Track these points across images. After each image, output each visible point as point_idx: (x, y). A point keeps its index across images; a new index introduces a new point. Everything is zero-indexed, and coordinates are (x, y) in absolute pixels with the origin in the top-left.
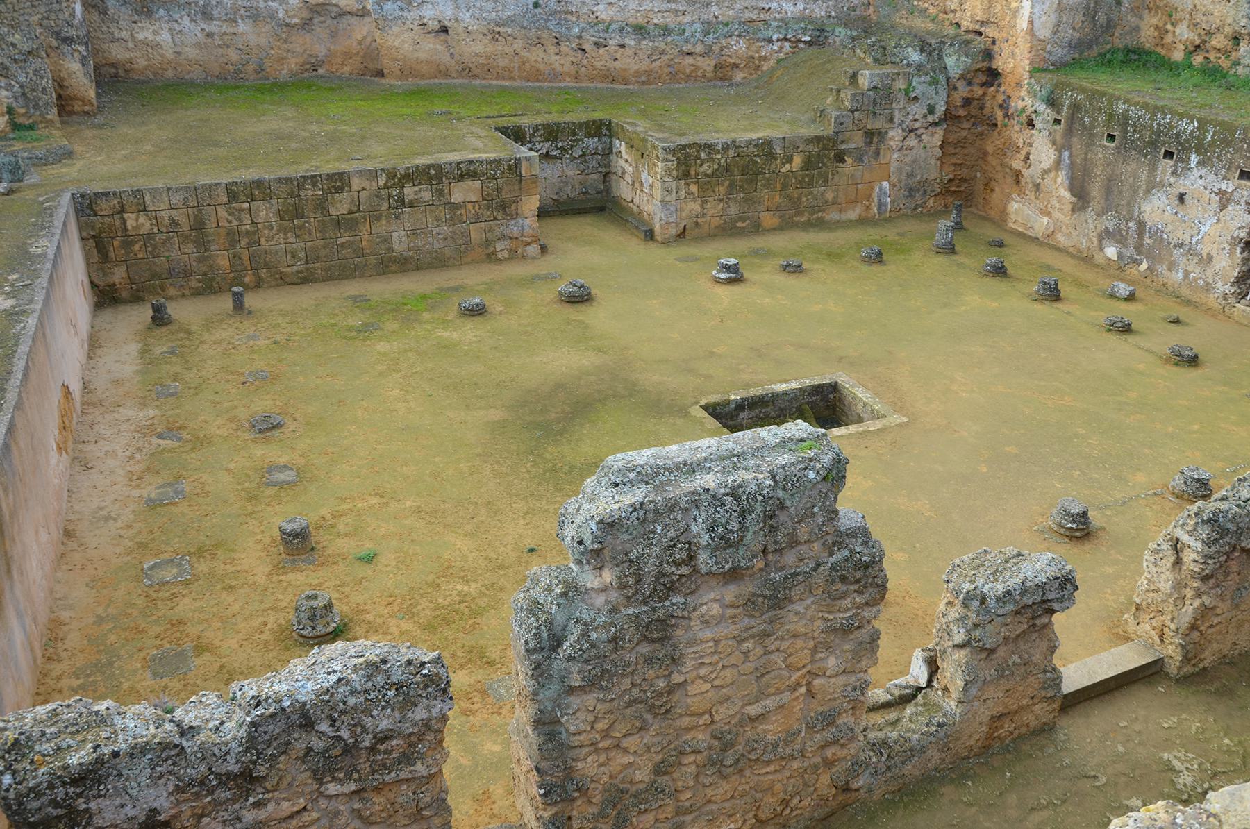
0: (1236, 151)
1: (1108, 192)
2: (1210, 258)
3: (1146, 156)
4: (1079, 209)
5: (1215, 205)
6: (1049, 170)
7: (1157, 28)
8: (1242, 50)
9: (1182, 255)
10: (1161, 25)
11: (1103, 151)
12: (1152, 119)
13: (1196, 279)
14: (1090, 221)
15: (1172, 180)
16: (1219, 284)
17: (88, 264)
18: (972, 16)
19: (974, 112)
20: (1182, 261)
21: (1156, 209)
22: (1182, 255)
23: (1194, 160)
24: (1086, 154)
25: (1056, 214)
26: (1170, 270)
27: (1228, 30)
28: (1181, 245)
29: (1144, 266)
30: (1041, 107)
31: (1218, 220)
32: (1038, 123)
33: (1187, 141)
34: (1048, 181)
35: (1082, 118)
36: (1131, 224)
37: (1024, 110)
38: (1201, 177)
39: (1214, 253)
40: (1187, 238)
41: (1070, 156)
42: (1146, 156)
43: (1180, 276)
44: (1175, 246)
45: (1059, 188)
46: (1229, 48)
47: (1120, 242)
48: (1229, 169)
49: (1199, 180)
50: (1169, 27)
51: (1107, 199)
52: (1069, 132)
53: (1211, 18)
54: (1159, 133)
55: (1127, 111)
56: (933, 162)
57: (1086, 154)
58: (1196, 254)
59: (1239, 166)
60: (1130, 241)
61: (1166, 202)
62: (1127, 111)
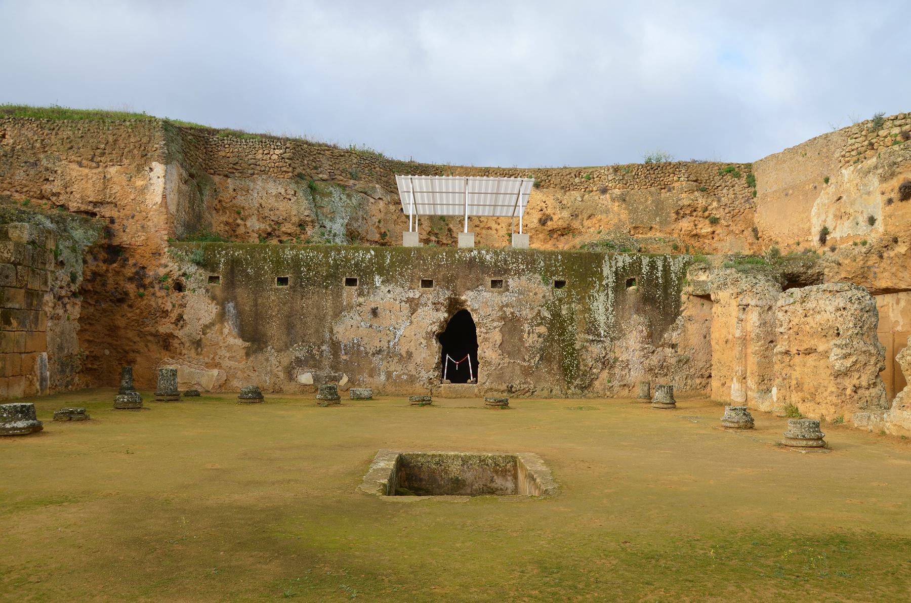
1: (289, 327)
2: (410, 355)
3: (327, 288)
4: (255, 352)
6: (212, 324)
7: (227, 223)
8: (309, 233)
9: (382, 360)
10: (231, 221)
11: (274, 296)
13: (399, 376)
14: (272, 359)
15: (361, 300)
16: (423, 373)
18: (82, 198)
19: (99, 288)
20: (383, 366)
21: (349, 329)
22: (382, 360)
23: (378, 280)
24: (256, 300)
25: (227, 363)
26: (371, 376)
27: (295, 219)
29: (345, 379)
30: (192, 269)
31: (411, 322)
32: (190, 284)
33: (367, 267)
34: (212, 334)
35: (245, 270)
36: (324, 348)
37: (168, 275)
38: (389, 291)
39: (413, 349)
40: (384, 344)
41: (236, 307)
42: (327, 288)
43: (383, 377)
44: (373, 354)
45: (229, 338)
46: (298, 232)
47: (314, 366)
49: (386, 295)
50: (239, 221)
51: (288, 334)
52: (231, 284)
53: (277, 212)
54: (336, 266)
55: (297, 255)
56: (74, 335)
57: (256, 300)
58: (396, 355)
59: (420, 277)
61: (359, 319)
62: (297, 255)
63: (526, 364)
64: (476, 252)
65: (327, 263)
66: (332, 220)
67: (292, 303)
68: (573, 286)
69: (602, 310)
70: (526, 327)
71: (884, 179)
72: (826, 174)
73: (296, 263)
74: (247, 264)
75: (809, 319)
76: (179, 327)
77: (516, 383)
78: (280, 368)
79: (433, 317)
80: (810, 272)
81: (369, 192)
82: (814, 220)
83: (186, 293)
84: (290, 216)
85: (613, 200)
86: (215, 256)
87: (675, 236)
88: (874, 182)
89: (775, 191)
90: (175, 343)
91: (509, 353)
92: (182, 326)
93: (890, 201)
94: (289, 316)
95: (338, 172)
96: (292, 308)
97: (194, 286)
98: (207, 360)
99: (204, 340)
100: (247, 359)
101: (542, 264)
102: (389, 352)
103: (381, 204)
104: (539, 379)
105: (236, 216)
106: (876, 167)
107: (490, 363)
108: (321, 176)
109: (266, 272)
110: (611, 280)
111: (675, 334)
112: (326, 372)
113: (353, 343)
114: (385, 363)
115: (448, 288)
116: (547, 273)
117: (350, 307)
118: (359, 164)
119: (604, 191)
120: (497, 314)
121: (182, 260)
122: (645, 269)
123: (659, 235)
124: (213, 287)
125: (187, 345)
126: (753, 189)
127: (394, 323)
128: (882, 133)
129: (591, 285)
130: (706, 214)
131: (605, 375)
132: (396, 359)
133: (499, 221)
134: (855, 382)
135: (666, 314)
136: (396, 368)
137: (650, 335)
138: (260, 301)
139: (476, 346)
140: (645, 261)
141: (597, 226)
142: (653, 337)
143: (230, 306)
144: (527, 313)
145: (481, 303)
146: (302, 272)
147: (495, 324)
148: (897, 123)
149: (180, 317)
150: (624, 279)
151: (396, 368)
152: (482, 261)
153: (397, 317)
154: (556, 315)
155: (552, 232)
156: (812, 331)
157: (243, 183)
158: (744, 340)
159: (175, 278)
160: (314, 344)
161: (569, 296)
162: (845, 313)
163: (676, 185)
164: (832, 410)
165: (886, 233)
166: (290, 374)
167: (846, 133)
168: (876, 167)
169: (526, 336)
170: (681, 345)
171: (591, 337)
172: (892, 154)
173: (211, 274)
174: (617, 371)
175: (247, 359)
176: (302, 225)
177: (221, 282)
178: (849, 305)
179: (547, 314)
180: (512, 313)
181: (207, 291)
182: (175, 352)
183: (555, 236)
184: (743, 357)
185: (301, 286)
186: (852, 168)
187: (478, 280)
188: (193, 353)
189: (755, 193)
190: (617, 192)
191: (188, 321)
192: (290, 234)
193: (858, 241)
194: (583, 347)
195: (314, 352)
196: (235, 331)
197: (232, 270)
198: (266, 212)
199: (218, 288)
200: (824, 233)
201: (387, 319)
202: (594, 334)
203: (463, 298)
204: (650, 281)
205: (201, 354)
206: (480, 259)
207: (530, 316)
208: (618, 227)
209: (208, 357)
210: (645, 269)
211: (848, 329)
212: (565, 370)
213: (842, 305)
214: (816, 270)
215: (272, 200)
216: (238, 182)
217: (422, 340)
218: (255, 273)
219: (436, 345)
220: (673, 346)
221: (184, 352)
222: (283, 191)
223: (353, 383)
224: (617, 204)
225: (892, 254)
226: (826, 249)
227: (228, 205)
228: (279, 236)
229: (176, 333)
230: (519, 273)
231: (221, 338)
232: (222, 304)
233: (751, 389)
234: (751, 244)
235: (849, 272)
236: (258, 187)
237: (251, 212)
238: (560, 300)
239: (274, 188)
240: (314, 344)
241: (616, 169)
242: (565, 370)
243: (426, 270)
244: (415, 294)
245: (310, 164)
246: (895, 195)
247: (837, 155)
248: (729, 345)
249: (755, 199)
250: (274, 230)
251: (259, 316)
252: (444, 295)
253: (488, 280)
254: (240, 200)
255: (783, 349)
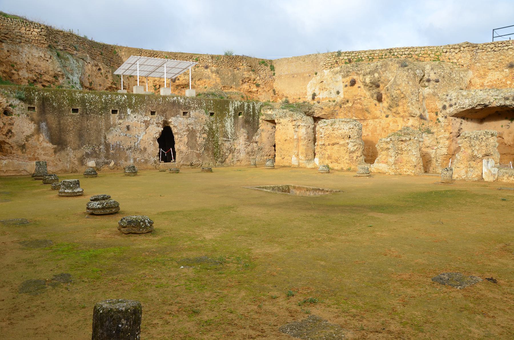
0: (147, 104)
1: (80, 136)
2: (145, 149)
3: (101, 115)
4: (59, 150)
5: (143, 127)
6: (32, 135)
7: (4, 72)
9: (131, 152)
10: (7, 70)
11: (70, 119)
12: (101, 98)
13: (140, 160)
15: (121, 121)
17: (359, 52)
20: (132, 155)
21: (114, 137)
22: (131, 152)
23: (129, 111)
24: (59, 121)
26: (126, 161)
28: (130, 148)
29: (113, 163)
30: (17, 102)
31: (146, 133)
32: (16, 111)
33: (123, 104)
35: (52, 104)
36: (101, 147)
41: (47, 125)
42: (101, 115)
43: (132, 161)
44: (127, 150)
45: (43, 144)
47: (96, 157)
48: (146, 112)
49: (134, 119)
50: (13, 71)
52: (43, 111)
53: (40, 68)
54: (106, 103)
55: (83, 96)
57: (59, 121)
60: (102, 155)
62: (83, 96)
63: (198, 152)
64: (175, 98)
65: (101, 101)
66: (72, 74)
67: (81, 123)
68: (217, 115)
69: (229, 126)
70: (198, 135)
71: (344, 77)
72: (316, 71)
73: (83, 101)
74: (52, 100)
75: (335, 132)
76: (8, 137)
77: (194, 161)
78: (76, 159)
79: (156, 130)
80: (310, 111)
81: (85, 59)
82: (309, 90)
83: (13, 116)
84: (48, 71)
85: (212, 72)
86: (31, 95)
87: (242, 91)
88: (339, 78)
89: (287, 75)
90: (7, 147)
91: (191, 147)
92: (10, 137)
93: (346, 86)
94: (80, 130)
95: (68, 46)
96: (81, 125)
97: (18, 112)
98: (29, 156)
99: (27, 145)
100: (55, 155)
101: (205, 104)
102: (135, 148)
103: (90, 65)
104: (204, 159)
105: (11, 68)
106: (340, 72)
107: (182, 152)
108: (59, 47)
109: (65, 105)
110: (232, 113)
111: (257, 137)
112: (102, 159)
113: (117, 144)
114: (133, 154)
115: (163, 116)
116: (207, 108)
117: (115, 125)
118: (77, 42)
119: (207, 67)
120: (185, 128)
121: (8, 96)
122: (246, 108)
123: (235, 90)
124: (31, 113)
125: (15, 147)
126: (273, 72)
127: (137, 133)
128: (341, 58)
129: (225, 115)
130: (255, 82)
131: (230, 156)
132: (138, 152)
133: (149, 78)
134: (357, 155)
135: (254, 128)
136: (139, 157)
137: (248, 138)
138: (62, 122)
139: (174, 143)
140: (246, 104)
141: (203, 84)
142: (249, 138)
143: (43, 125)
144: (199, 128)
145: (178, 124)
146: (86, 106)
147: (185, 133)
148: (347, 55)
149: (10, 131)
150: (238, 112)
151: (139, 157)
152: (179, 102)
153: (139, 130)
154: (211, 129)
155: (178, 86)
156: (336, 136)
157: (14, 47)
158: (298, 140)
159: (4, 107)
160: (95, 145)
161: (216, 120)
162: (353, 130)
163: (241, 67)
164: (347, 165)
165: (344, 98)
166: (82, 161)
167: (326, 55)
168: (340, 72)
169: (198, 139)
170: (260, 142)
171: (225, 139)
172: (347, 67)
173: (29, 106)
174: (235, 154)
175: (55, 155)
176: (56, 76)
177: (36, 110)
178: (355, 127)
179: (207, 128)
180: (192, 128)
181: (28, 115)
182: (7, 152)
183: (179, 88)
184: (298, 146)
185: (86, 113)
186: (329, 70)
187: (177, 112)
188: (20, 152)
189: (274, 74)
190: (214, 69)
191: (15, 134)
192: (49, 82)
193: (331, 100)
194: (222, 143)
195: (96, 149)
196: (47, 139)
197: (43, 104)
198: (33, 67)
199: (35, 114)
200: (314, 95)
201: (134, 131)
202: (227, 138)
203: (170, 120)
204: (248, 114)
205: (25, 153)
206: (178, 101)
207: (200, 129)
208: (216, 86)
209: (30, 154)
210: (246, 108)
211: (355, 136)
212: (215, 154)
213: (352, 127)
214: (312, 111)
215: (36, 61)
216: (10, 46)
217: (151, 142)
218: (58, 105)
219: (157, 144)
220: (256, 142)
221: (13, 152)
222: (43, 55)
223: (117, 165)
224: (214, 74)
225: (345, 106)
226: (315, 102)
227: (4, 60)
228: (41, 82)
229: (7, 140)
230: (195, 109)
231: (38, 143)
232: (38, 123)
233: (301, 160)
234: (272, 97)
235: (326, 112)
236: (25, 51)
237: (22, 66)
238: (212, 122)
239: (37, 53)
240: (95, 145)
241: (212, 57)
242: (214, 154)
243: (153, 106)
244: (148, 118)
245: (57, 41)
246: (348, 84)
247: (322, 63)
248: (287, 142)
249: (274, 77)
250: (38, 78)
251: (62, 130)
252: (161, 119)
253: (181, 112)
254: (13, 58)
255: (322, 143)
